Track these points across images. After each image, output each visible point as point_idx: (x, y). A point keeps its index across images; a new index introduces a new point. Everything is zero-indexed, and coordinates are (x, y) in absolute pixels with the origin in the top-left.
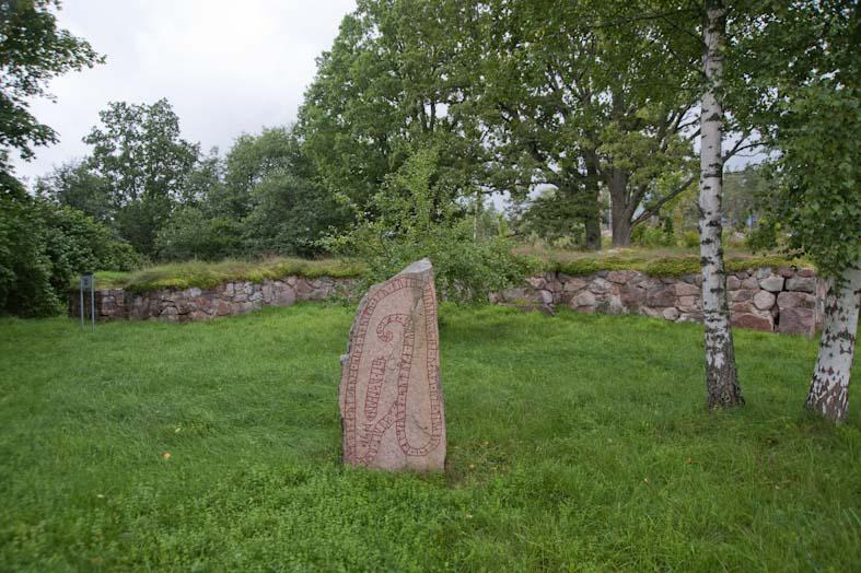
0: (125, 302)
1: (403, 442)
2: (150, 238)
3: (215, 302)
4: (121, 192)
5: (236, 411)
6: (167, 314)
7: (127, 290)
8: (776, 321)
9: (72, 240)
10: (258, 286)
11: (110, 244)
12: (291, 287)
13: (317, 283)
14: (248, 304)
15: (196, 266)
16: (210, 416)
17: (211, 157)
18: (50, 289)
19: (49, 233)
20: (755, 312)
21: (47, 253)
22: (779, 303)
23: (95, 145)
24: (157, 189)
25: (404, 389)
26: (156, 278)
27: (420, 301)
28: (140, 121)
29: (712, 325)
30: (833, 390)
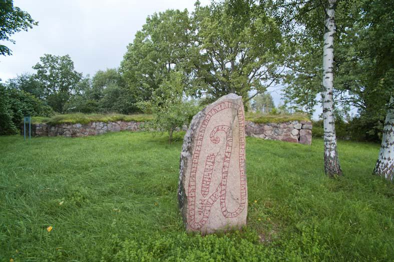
0: (47, 129)
1: (224, 209)
2: (61, 107)
3: (88, 130)
4: (49, 89)
5: (101, 185)
6: (66, 134)
7: (47, 124)
8: (299, 139)
9: (24, 104)
10: (105, 124)
11: (42, 107)
12: (119, 125)
13: (129, 124)
14: (101, 131)
15: (79, 115)
16: (85, 191)
17: (87, 78)
18: (12, 124)
19: (13, 100)
20: (292, 136)
21: (12, 108)
22: (300, 133)
23: (38, 70)
24: (64, 89)
25: (225, 174)
26: (61, 119)
27: (236, 117)
28: (57, 62)
29: (329, 138)
30: (390, 167)
